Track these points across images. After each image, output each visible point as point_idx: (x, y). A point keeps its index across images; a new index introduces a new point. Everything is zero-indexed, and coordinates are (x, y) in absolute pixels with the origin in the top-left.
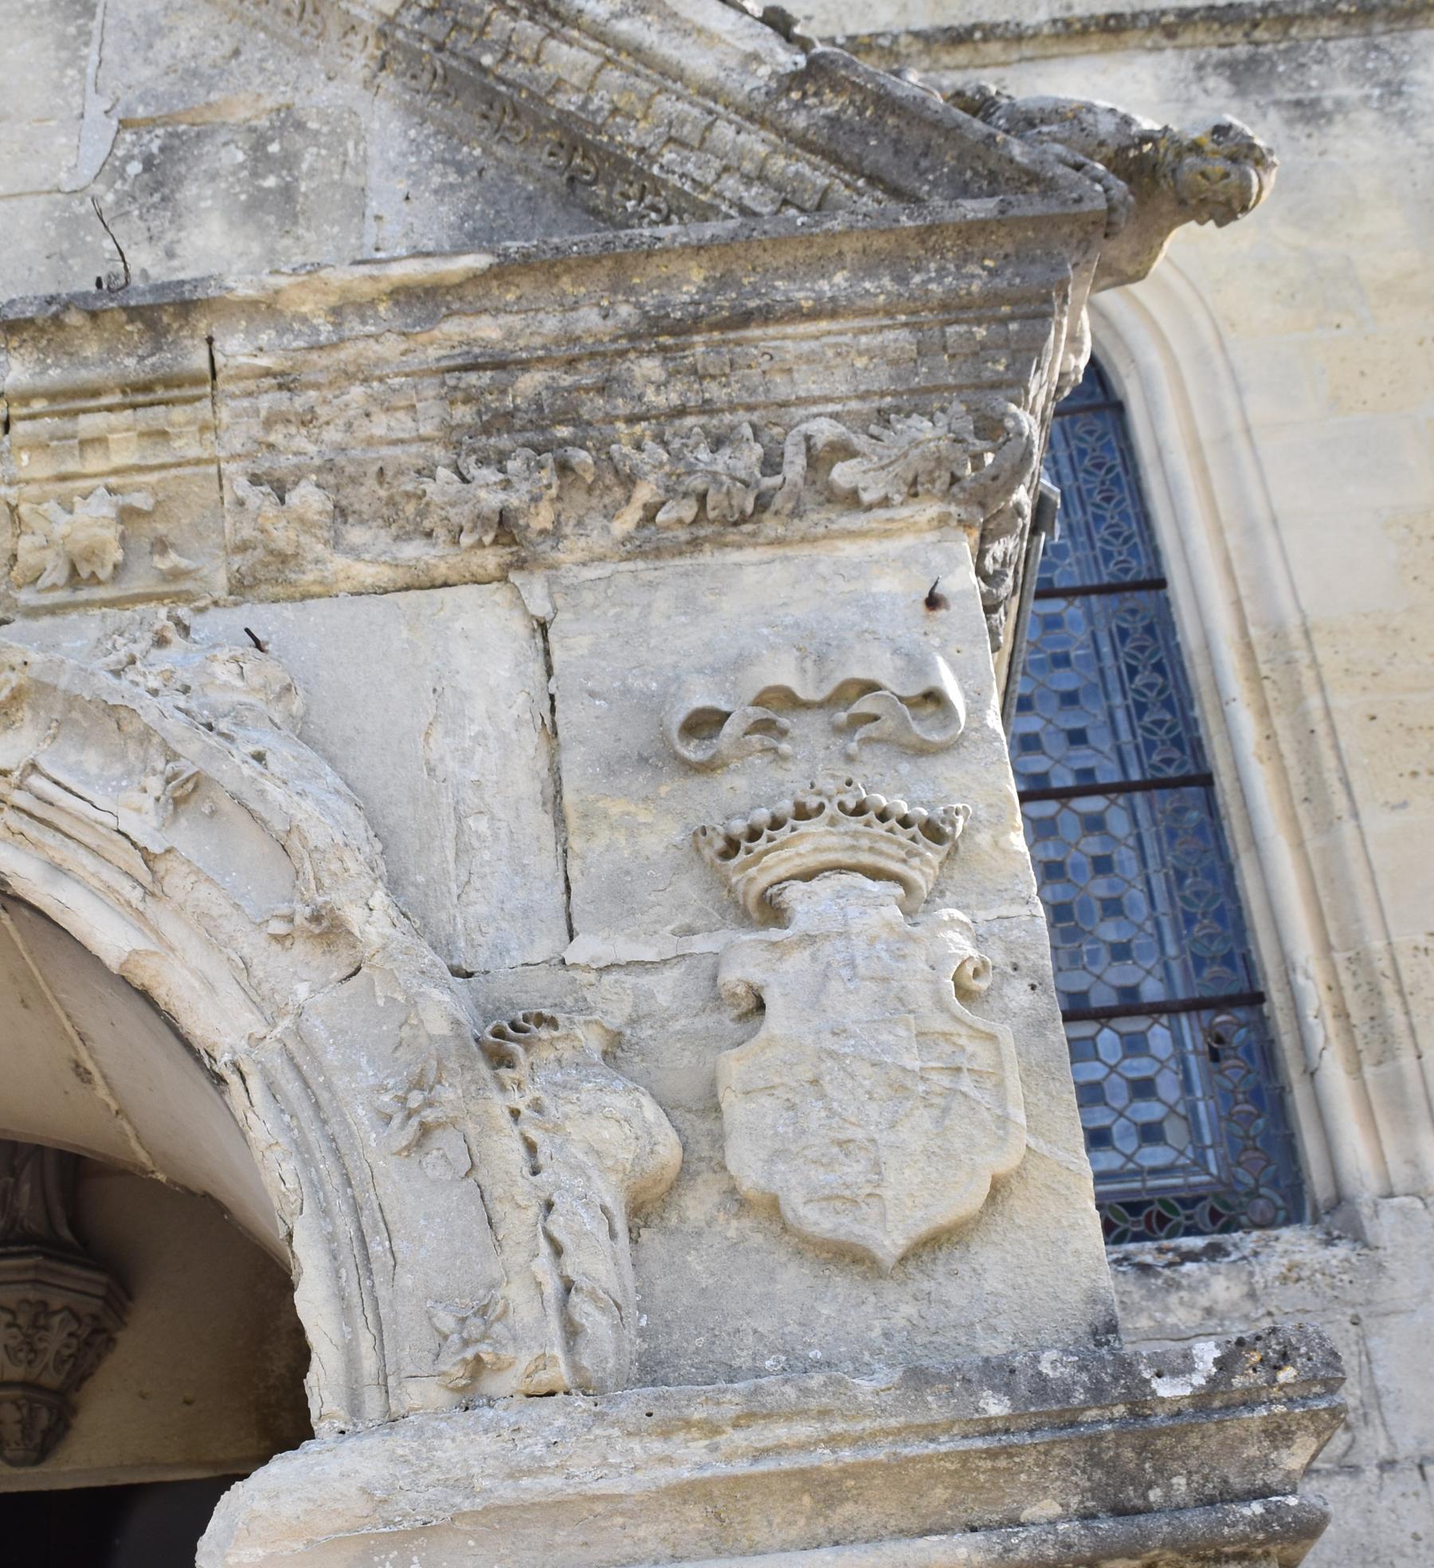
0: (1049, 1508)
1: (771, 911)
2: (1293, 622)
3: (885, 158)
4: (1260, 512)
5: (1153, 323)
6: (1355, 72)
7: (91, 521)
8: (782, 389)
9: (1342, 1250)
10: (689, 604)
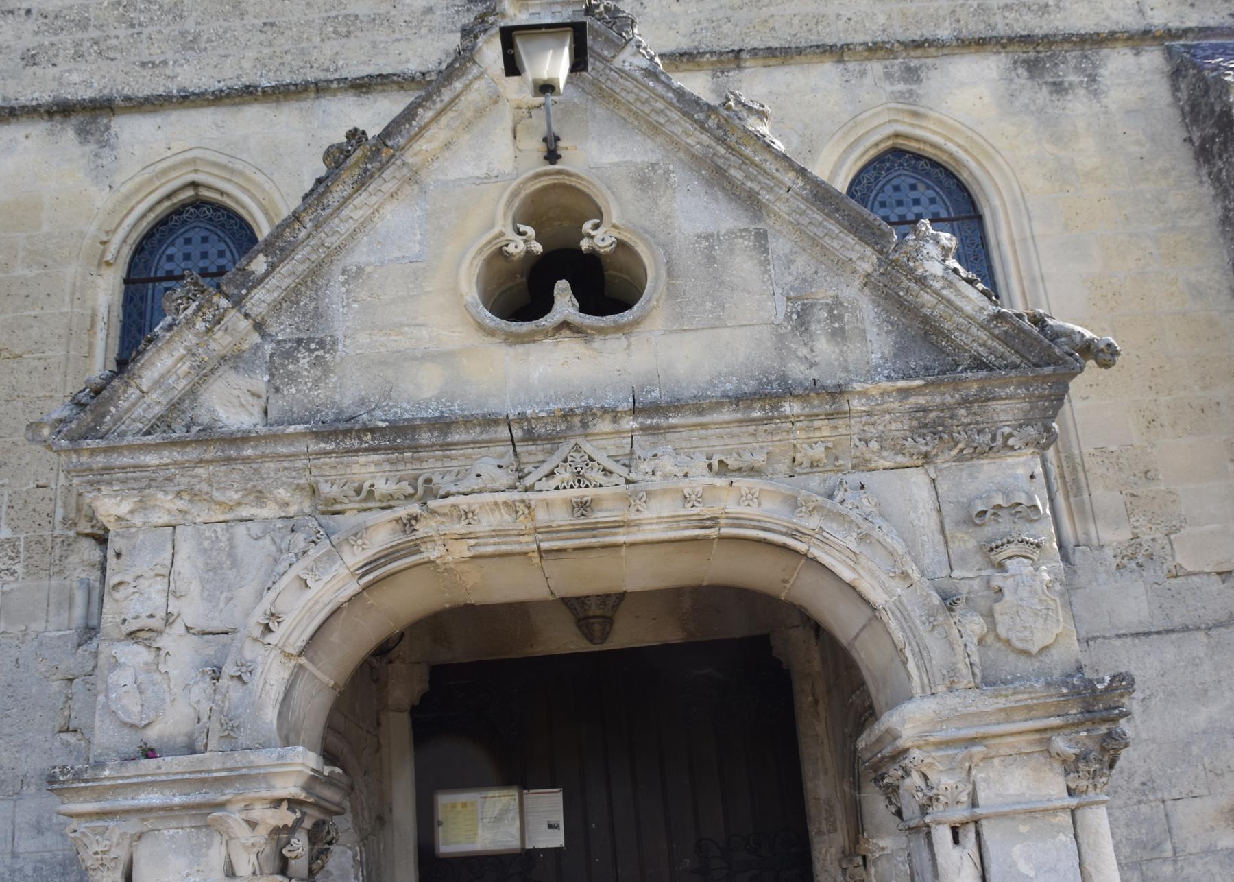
0: (1074, 711)
1: (1001, 567)
3: (1020, 347)
4: (1037, 274)
5: (996, 184)
6: (1078, 69)
7: (818, 452)
8: (996, 418)
10: (971, 475)
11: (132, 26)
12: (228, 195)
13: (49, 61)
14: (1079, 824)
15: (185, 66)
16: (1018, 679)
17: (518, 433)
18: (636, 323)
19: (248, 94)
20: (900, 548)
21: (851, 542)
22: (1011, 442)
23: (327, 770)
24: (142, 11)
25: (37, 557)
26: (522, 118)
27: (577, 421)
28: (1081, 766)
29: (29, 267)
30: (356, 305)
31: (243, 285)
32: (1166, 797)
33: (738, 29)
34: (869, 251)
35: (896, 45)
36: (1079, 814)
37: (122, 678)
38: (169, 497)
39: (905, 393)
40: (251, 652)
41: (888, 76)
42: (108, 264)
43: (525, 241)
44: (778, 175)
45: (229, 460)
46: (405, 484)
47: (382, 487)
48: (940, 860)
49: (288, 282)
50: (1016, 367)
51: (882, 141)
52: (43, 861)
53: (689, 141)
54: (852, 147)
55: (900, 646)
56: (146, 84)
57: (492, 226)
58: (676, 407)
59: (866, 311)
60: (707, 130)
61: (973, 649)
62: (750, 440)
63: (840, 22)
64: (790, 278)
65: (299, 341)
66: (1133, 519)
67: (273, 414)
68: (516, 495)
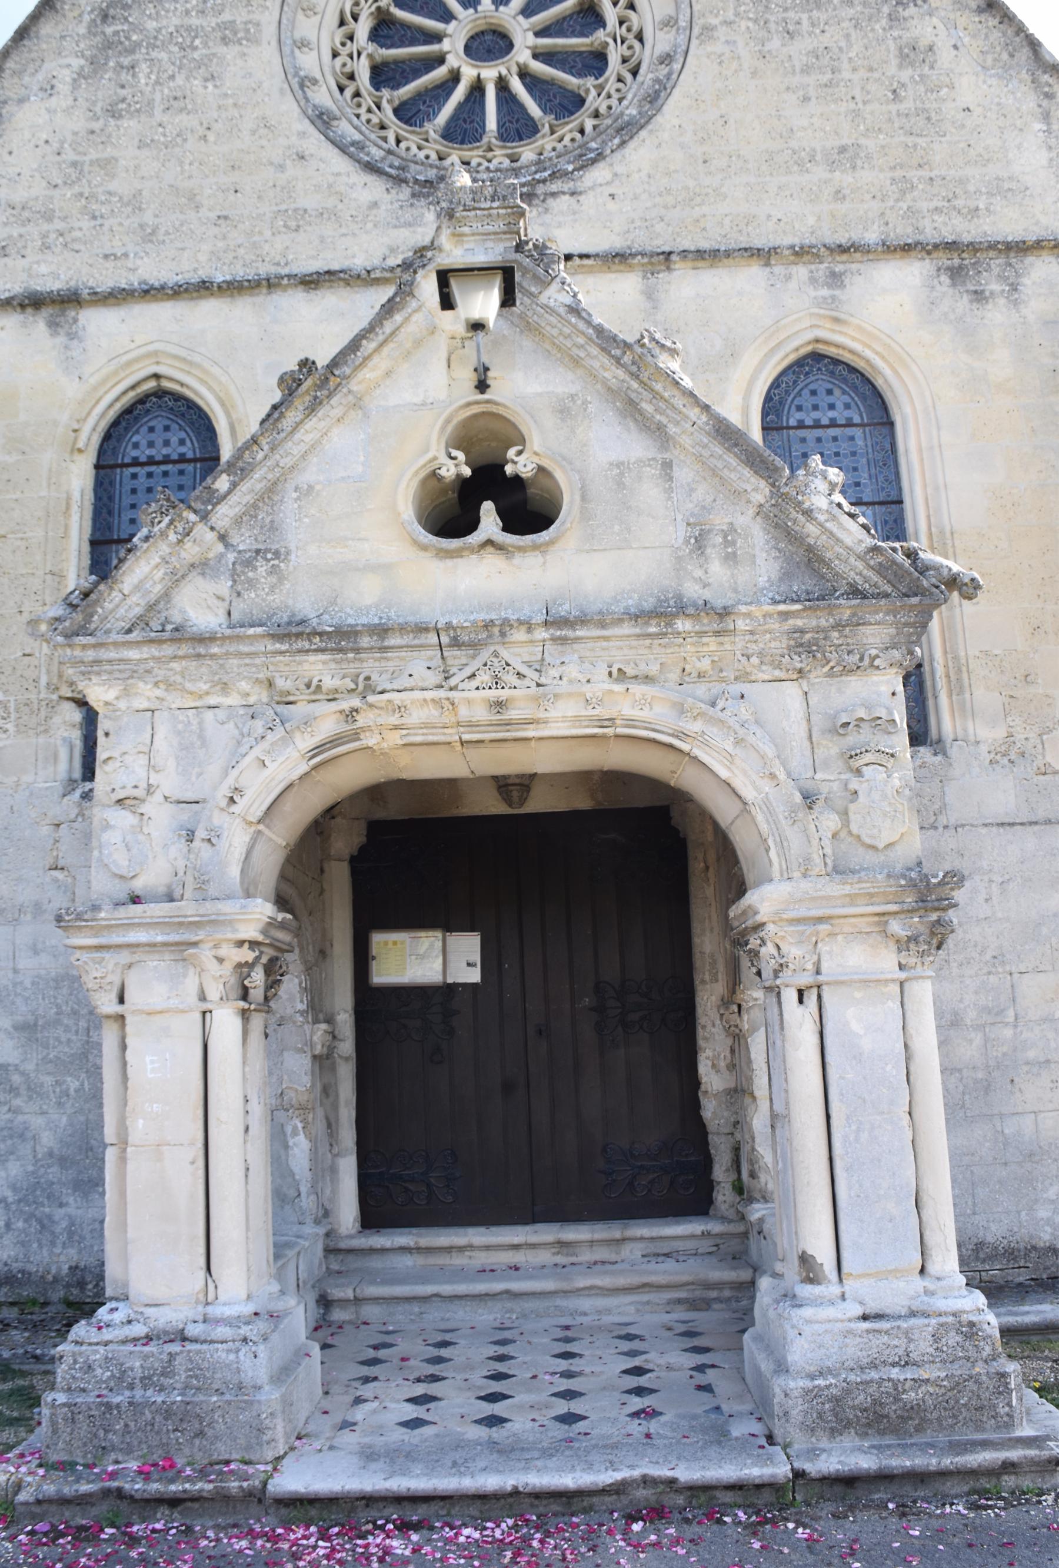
1: (858, 772)
2: (948, 529)
5: (909, 392)
6: (1001, 278)
7: (705, 664)
9: (939, 758)
10: (839, 690)
11: (94, 218)
12: (188, 387)
13: (18, 252)
14: (906, 994)
15: (146, 259)
16: (864, 869)
17: (445, 640)
18: (552, 542)
19: (204, 288)
20: (770, 751)
21: (729, 745)
22: (877, 662)
23: (280, 916)
24: (103, 203)
25: (25, 718)
26: (456, 348)
27: (496, 630)
28: (912, 946)
29: (9, 453)
30: (306, 520)
31: (209, 501)
32: (1014, 970)
33: (670, 229)
34: (763, 484)
35: (823, 249)
36: (906, 985)
37: (113, 837)
38: (149, 686)
39: (785, 615)
40: (218, 819)
41: (813, 280)
42: (80, 451)
43: (456, 465)
44: (684, 410)
45: (199, 656)
46: (348, 680)
47: (328, 683)
48: (786, 1016)
49: (249, 498)
50: (887, 596)
51: (802, 346)
52: (39, 976)
53: (606, 375)
54: (773, 351)
55: (765, 836)
56: (107, 278)
57: (427, 450)
58: (582, 622)
59: (757, 538)
60: (622, 366)
61: (826, 842)
62: (646, 651)
63: (770, 224)
64: (691, 505)
65: (258, 551)
66: (1009, 719)
67: (236, 616)
68: (442, 694)
